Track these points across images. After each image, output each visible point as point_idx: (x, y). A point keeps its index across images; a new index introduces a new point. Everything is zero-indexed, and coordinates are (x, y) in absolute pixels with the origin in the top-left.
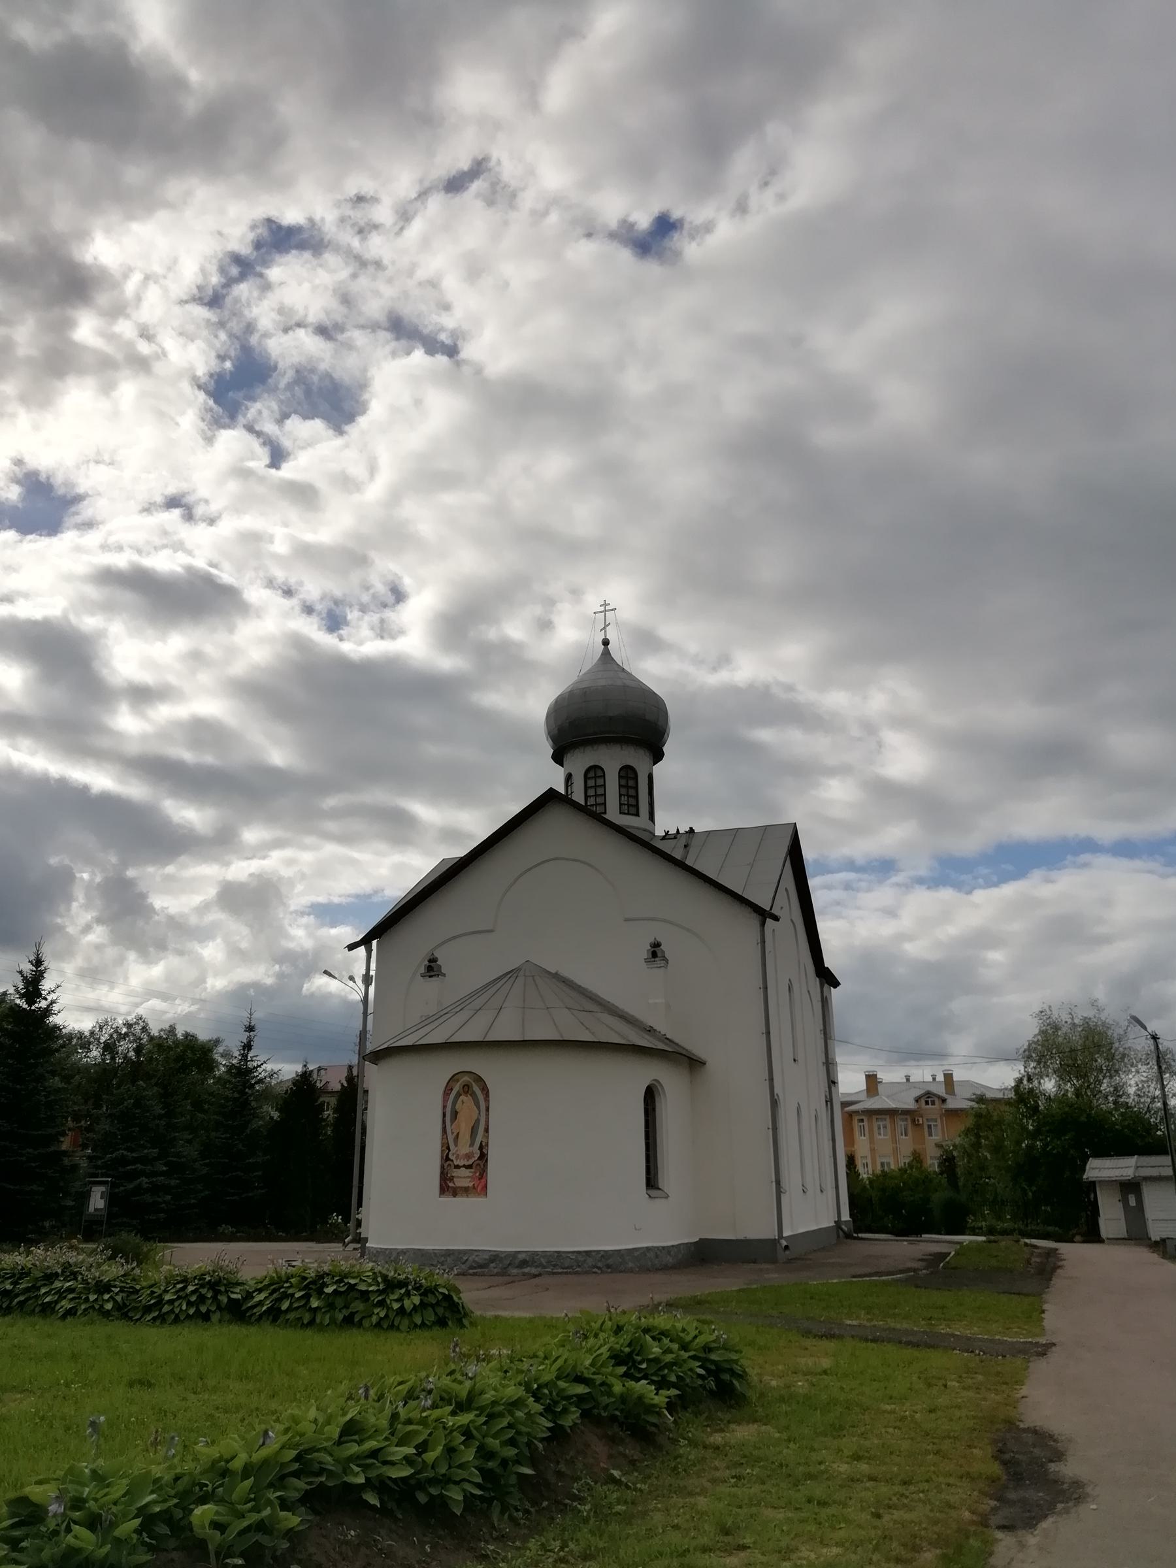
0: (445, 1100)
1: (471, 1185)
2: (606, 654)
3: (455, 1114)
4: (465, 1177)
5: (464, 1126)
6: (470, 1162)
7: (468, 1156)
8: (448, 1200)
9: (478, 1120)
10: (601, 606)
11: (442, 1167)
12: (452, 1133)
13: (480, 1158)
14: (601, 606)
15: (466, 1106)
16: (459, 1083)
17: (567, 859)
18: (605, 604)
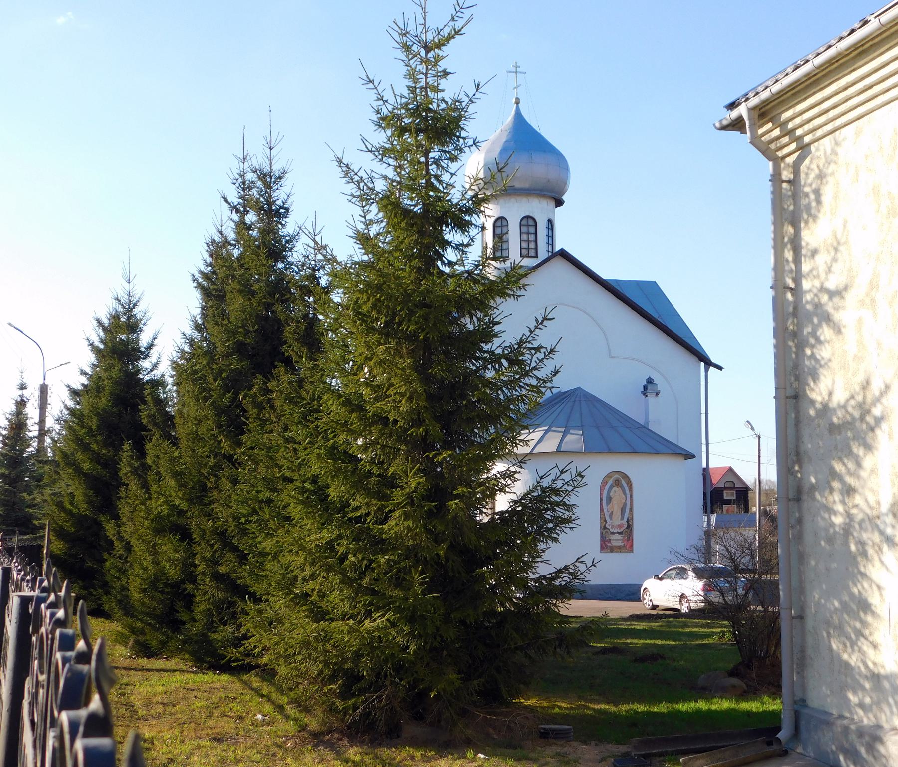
0: (602, 490)
1: (622, 544)
3: (609, 499)
5: (616, 507)
6: (621, 530)
7: (620, 526)
9: (625, 504)
11: (602, 533)
13: (627, 528)
14: (513, 66)
15: (617, 493)
18: (517, 67)
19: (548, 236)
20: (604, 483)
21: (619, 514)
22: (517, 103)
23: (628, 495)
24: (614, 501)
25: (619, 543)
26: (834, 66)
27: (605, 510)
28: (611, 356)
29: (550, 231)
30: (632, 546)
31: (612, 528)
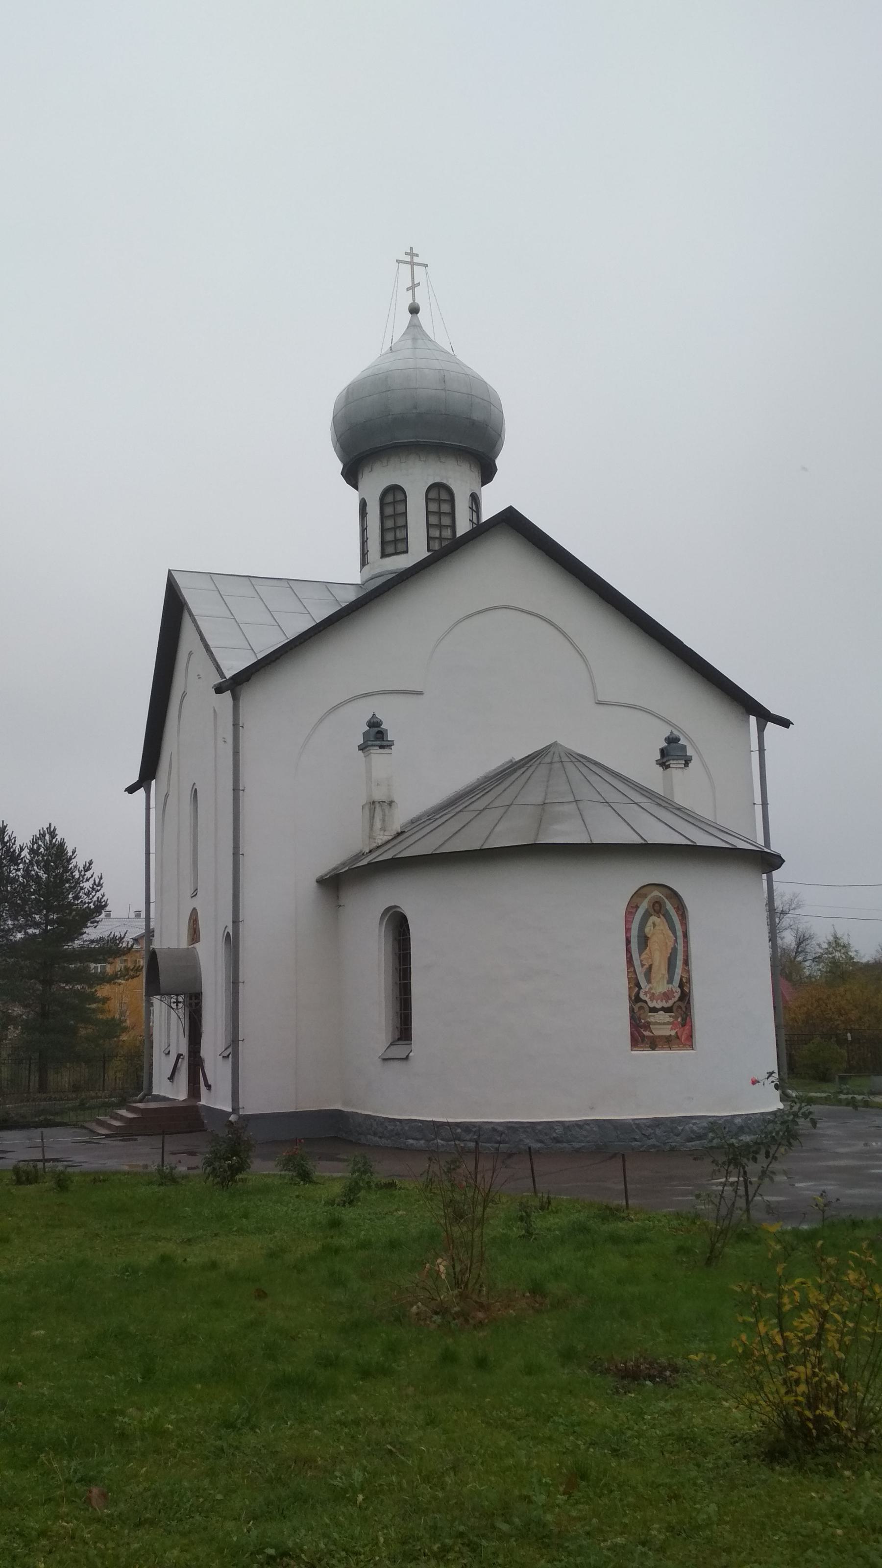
0: (628, 922)
1: (673, 1033)
2: (414, 328)
3: (644, 941)
4: (664, 1024)
5: (658, 955)
6: (670, 1004)
7: (666, 996)
8: (645, 1054)
9: (674, 950)
10: (406, 254)
11: (632, 1010)
12: (643, 965)
13: (681, 999)
14: (406, 254)
15: (657, 928)
16: (646, 900)
17: (522, 611)
18: (411, 254)
19: (471, 508)
20: (632, 909)
21: (664, 971)
22: (414, 310)
23: (680, 934)
24: (654, 944)
25: (667, 1031)
26: (482, 786)
27: (637, 963)
28: (600, 703)
29: (475, 514)
30: (690, 1036)
31: (652, 999)
